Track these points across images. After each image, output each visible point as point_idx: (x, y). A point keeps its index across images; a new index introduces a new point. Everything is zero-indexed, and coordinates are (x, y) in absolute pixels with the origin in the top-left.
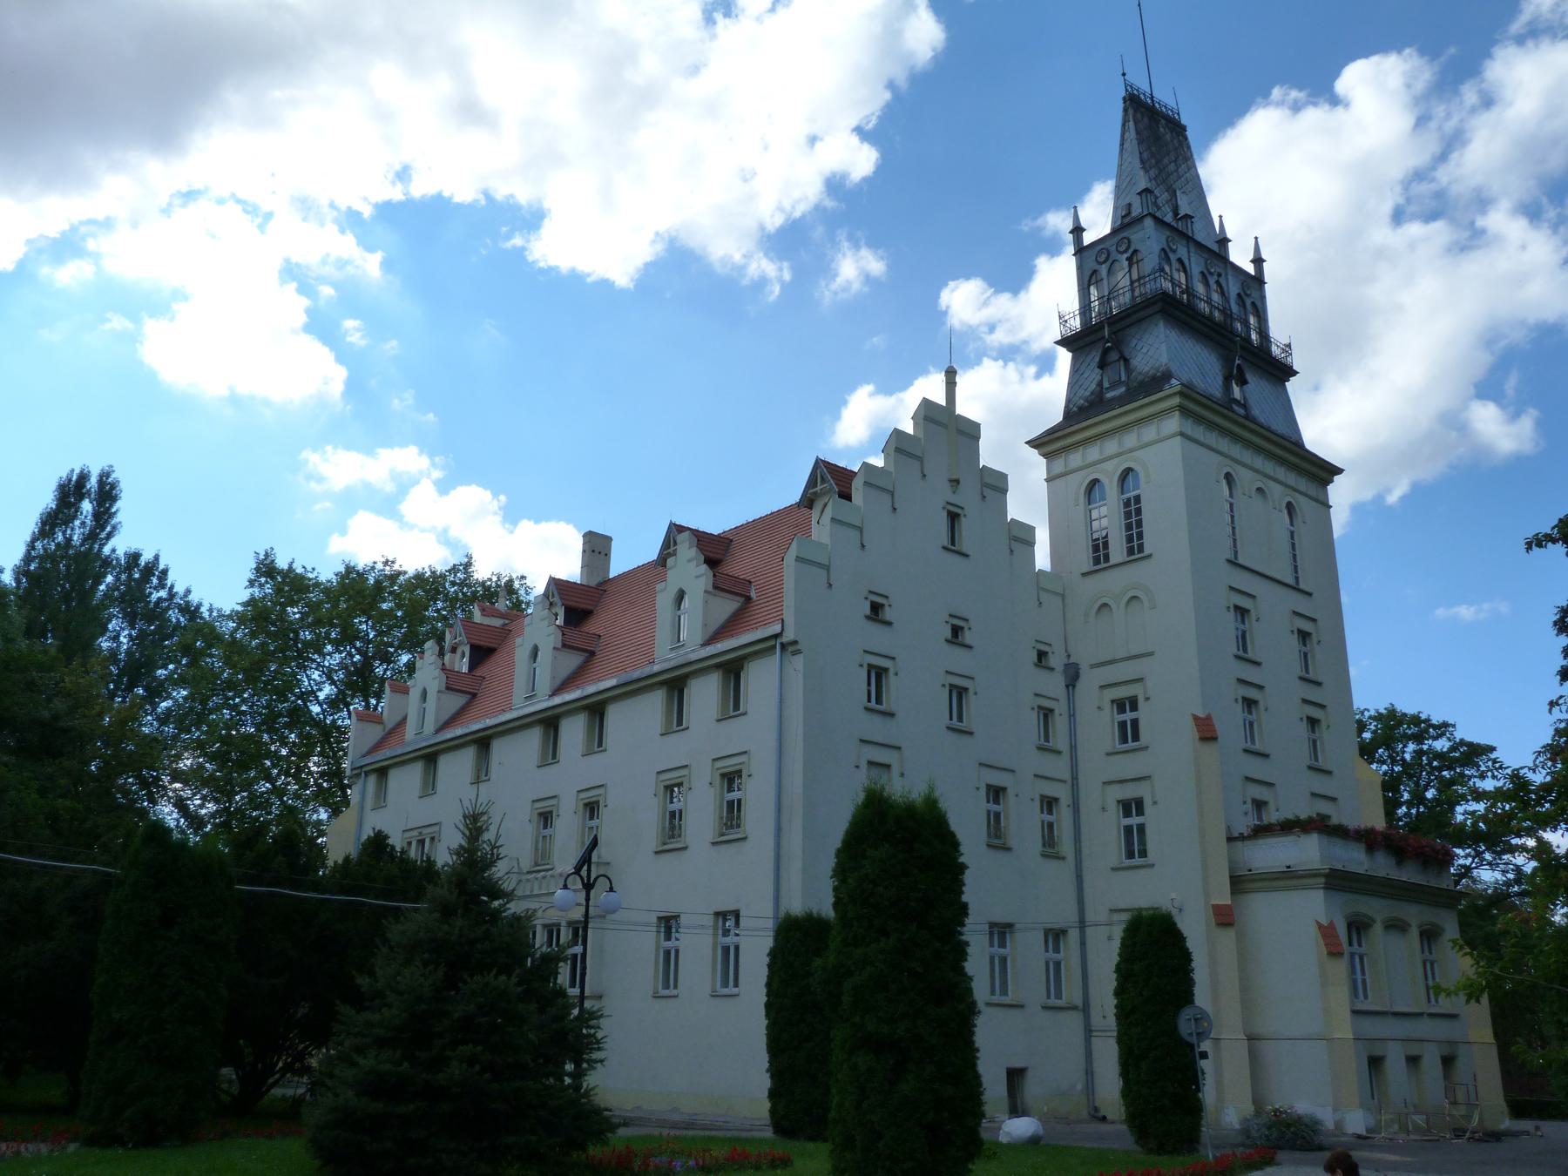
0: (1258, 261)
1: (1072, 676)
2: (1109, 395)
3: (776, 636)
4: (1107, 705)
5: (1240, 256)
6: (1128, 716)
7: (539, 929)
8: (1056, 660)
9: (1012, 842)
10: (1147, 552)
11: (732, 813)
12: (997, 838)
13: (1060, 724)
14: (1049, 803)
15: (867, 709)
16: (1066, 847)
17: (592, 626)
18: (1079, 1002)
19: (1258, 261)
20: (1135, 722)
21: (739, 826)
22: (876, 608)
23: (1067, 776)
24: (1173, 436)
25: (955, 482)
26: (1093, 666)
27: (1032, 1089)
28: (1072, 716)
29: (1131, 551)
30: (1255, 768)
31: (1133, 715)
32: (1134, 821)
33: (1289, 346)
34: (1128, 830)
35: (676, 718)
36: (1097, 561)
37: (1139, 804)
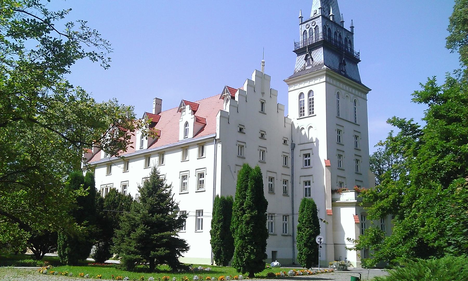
0: (352, 27)
1: (293, 147)
2: (307, 68)
3: (214, 137)
4: (302, 156)
5: (347, 26)
8: (289, 143)
9: (266, 161)
11: (201, 183)
13: (289, 161)
14: (285, 182)
16: (290, 193)
17: (157, 127)
19: (352, 27)
23: (290, 174)
24: (324, 82)
25: (263, 93)
26: (299, 145)
27: (278, 256)
29: (310, 113)
30: (357, 153)
33: (359, 53)
34: (306, 189)
35: (184, 158)
36: (301, 115)
37: (309, 182)
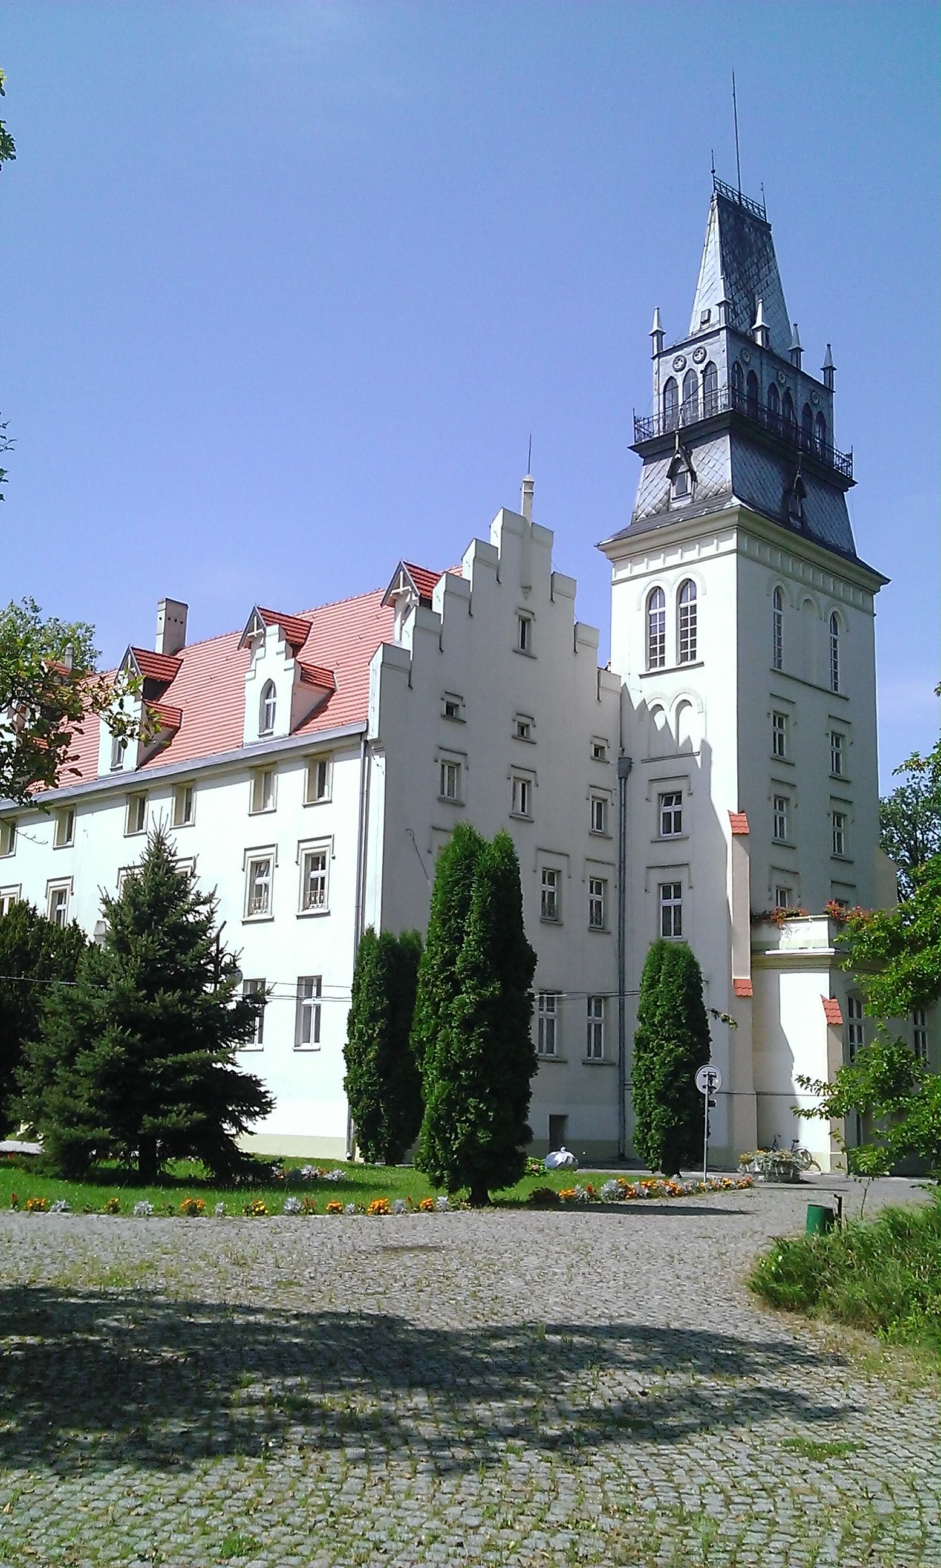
0: (829, 370)
4: (655, 798)
5: (811, 366)
6: (672, 809)
7: (431, 1073)
8: (611, 754)
10: (698, 660)
11: (314, 889)
12: (551, 912)
13: (612, 814)
14: (598, 885)
15: (440, 800)
16: (612, 924)
18: (614, 1057)
19: (829, 370)
20: (678, 814)
21: (321, 902)
22: (451, 709)
23: (614, 858)
24: (731, 552)
26: (644, 761)
27: (572, 1132)
28: (623, 805)
29: (684, 657)
31: (677, 808)
32: (672, 902)
33: (850, 456)
35: (260, 804)
36: (652, 663)
37: (678, 887)
